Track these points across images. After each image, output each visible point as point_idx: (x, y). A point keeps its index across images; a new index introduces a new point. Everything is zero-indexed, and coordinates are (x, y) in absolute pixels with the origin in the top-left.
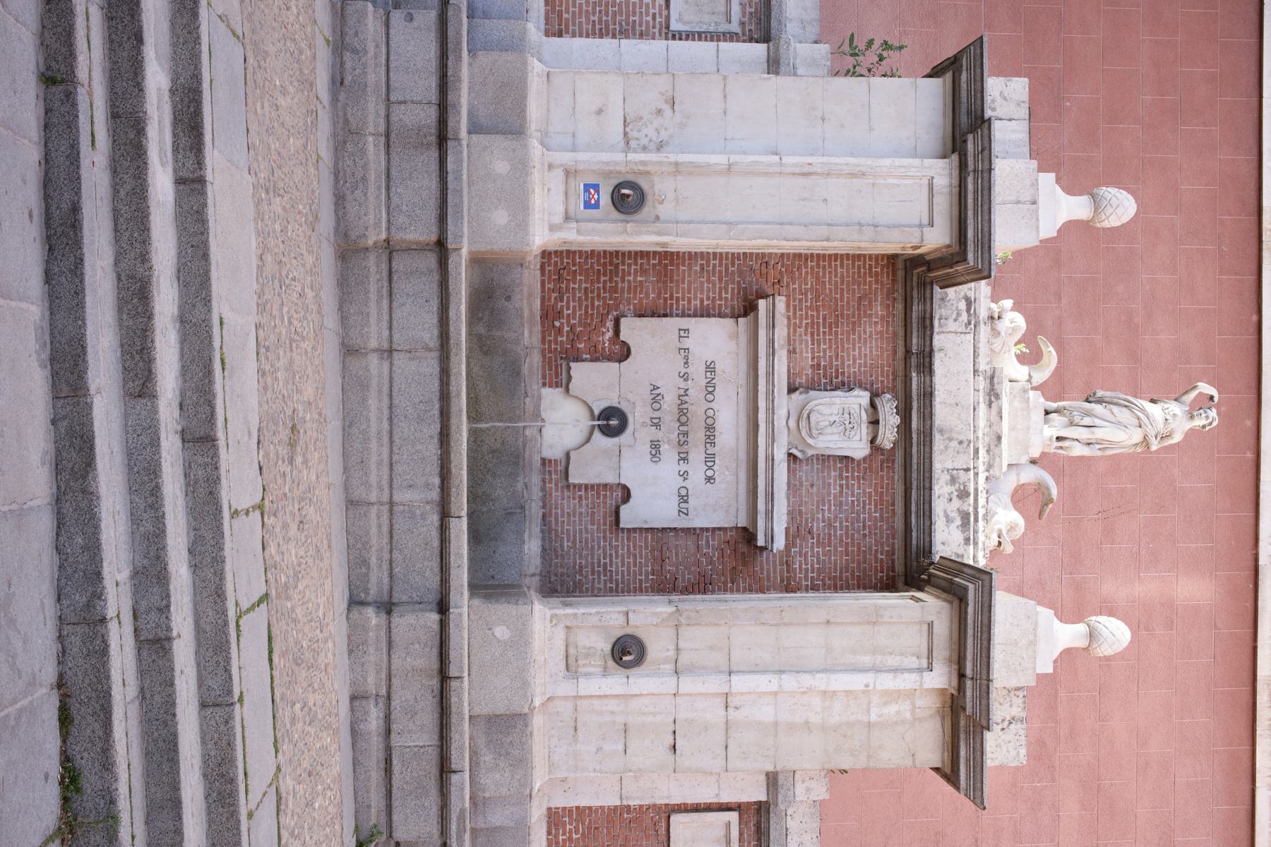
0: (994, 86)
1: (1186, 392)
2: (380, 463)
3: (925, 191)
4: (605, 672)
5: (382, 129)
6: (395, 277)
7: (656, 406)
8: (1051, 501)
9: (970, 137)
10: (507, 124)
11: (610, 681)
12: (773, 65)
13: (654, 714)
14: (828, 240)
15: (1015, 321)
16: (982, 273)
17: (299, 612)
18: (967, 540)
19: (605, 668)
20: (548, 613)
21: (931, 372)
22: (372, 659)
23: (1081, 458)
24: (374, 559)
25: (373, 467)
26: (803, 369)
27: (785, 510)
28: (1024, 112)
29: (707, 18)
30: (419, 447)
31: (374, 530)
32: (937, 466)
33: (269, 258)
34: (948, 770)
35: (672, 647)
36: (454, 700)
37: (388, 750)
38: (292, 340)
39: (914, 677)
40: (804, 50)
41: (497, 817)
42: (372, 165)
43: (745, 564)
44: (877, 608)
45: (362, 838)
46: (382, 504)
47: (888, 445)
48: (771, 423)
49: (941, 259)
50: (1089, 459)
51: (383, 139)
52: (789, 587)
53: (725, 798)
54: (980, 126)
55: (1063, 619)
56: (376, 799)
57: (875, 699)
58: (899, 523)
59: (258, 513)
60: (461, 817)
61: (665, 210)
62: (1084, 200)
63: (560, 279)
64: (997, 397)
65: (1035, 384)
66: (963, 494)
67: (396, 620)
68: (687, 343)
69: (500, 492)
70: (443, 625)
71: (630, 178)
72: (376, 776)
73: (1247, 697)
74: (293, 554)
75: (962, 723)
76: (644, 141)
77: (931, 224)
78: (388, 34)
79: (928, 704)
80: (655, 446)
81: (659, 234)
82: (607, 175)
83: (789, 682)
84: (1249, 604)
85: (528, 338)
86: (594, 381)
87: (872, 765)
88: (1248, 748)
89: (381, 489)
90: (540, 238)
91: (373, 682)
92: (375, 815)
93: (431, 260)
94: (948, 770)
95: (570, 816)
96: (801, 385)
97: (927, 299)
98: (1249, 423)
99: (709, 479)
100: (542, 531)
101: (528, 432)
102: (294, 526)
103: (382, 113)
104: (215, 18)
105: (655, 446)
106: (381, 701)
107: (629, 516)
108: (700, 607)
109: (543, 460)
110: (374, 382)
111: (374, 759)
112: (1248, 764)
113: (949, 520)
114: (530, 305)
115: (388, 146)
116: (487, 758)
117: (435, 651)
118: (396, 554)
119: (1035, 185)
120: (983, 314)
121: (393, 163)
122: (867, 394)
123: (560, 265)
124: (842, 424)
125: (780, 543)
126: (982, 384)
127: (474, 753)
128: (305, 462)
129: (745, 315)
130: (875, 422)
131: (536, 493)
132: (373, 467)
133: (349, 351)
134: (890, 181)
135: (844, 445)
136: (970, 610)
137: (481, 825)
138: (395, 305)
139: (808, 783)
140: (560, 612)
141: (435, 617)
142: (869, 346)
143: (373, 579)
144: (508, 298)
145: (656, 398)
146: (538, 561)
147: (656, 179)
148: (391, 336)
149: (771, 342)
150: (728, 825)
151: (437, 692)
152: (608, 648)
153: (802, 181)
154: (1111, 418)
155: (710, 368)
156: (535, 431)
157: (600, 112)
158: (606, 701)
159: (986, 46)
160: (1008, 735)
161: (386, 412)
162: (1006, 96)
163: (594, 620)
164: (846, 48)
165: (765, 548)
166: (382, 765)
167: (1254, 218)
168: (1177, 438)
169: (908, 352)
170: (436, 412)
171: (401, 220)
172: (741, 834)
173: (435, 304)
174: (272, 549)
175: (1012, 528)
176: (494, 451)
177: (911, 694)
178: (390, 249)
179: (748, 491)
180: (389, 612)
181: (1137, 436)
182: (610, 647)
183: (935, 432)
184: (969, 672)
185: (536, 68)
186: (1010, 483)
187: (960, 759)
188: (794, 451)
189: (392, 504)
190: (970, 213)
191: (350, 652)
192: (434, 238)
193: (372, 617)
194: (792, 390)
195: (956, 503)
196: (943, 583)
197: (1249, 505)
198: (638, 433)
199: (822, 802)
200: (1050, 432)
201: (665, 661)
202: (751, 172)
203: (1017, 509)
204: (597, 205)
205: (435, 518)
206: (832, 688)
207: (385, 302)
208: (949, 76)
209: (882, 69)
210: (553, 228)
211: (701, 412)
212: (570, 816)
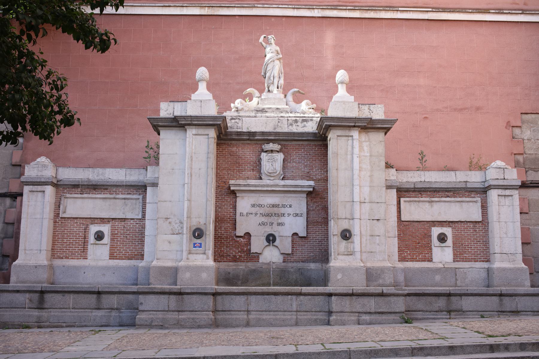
0: (163, 114)
1: (263, 46)
2: (284, 315)
3: (197, 136)
4: (353, 242)
5: (177, 313)
6: (224, 309)
7: (266, 224)
8: (298, 91)
9: (180, 122)
11: (355, 241)
12: (155, 185)
13: (367, 226)
15: (238, 103)
17: (328, 336)
18: (311, 120)
19: (351, 242)
20: (333, 261)
21: (255, 132)
22: (346, 318)
23: (285, 80)
24: (314, 317)
25: (285, 317)
26: (254, 175)
27: (301, 181)
28: (172, 104)
29: (137, 206)
30: (279, 302)
31: (305, 317)
33: (223, 343)
35: (345, 220)
36: (359, 292)
37: (376, 313)
39: (355, 142)
40: (150, 174)
41: (401, 278)
42: (189, 316)
43: (319, 195)
44: (332, 154)
45: (404, 321)
46: (297, 314)
47: (280, 146)
49: (218, 130)
50: (285, 76)
51: (180, 313)
52: (326, 180)
54: (177, 119)
55: (337, 91)
56: (392, 317)
57: (362, 154)
58: (306, 143)
60: (397, 290)
61: (202, 221)
62: (200, 84)
63: (223, 256)
64: (263, 109)
65: (259, 95)
66: (296, 121)
67: (334, 310)
68: (245, 213)
69: (294, 277)
70: (336, 295)
71: (192, 233)
72: (384, 317)
73: (367, 21)
74: (310, 338)
75: (370, 126)
76: (179, 228)
77: (208, 135)
78: (146, 311)
79: (364, 136)
80: (279, 224)
81: (210, 224)
82: (190, 240)
83: (356, 182)
84: (335, 20)
85: (242, 267)
86: (257, 244)
87: (384, 155)
88: (384, 21)
89: (292, 315)
90: (211, 262)
91: (354, 318)
92: (397, 317)
93: (219, 298)
94: (385, 130)
95: (402, 254)
96: (259, 175)
98: (273, 19)
99: (290, 206)
100: (307, 262)
101: (274, 267)
102: (302, 338)
103: (172, 313)
105: (279, 224)
106: (360, 315)
107: (303, 233)
108: (332, 212)
109: (283, 262)
110: (258, 316)
112: (389, 21)
113: (305, 126)
114: (231, 266)
115: (182, 311)
116: (381, 281)
117: (344, 297)
118: (313, 310)
119: (195, 101)
120: (236, 114)
121: (188, 309)
122: (263, 154)
123: (218, 257)
124: (272, 162)
125: (312, 183)
126: (259, 115)
127: (379, 285)
129: (236, 194)
130: (272, 151)
131: (295, 264)
132: (285, 317)
133: (248, 324)
134: (194, 148)
135: (279, 161)
136: (333, 124)
137: (403, 284)
138: (233, 310)
139: (391, 176)
140: (333, 257)
141: (333, 297)
142: (247, 153)
143: (321, 317)
144: (229, 273)
145: (263, 224)
146: (317, 264)
147: (192, 224)
148: (243, 311)
149: (245, 186)
150: (405, 201)
151: (357, 297)
154: (271, 70)
155: (253, 206)
156: (274, 265)
157: (170, 242)
158: (362, 242)
159: (151, 117)
160: (374, 110)
161: (267, 313)
162: (166, 110)
163: (336, 246)
164: (148, 160)
165: (314, 188)
166: (381, 315)
167: (203, 17)
168: (278, 48)
169: (248, 140)
170: (267, 297)
171: (206, 307)
173: (233, 297)
174: (308, 343)
175: (307, 104)
176: (280, 279)
177: (360, 142)
178: (215, 311)
179: (294, 193)
180: (332, 312)
181: (277, 62)
182: (345, 241)
183: (275, 131)
184: (353, 124)
185: (155, 263)
186: (292, 104)
187: (382, 127)
189: (297, 311)
190: (205, 123)
191: (344, 325)
192: (212, 297)
193: (333, 318)
194: (261, 178)
195: (299, 124)
196: (325, 130)
197: (301, 19)
198: (275, 230)
200: (275, 91)
201: (349, 222)
202: (190, 193)
203: (301, 102)
204: (200, 244)
205: (302, 297)
206: (358, 168)
207: (232, 313)
208: (159, 128)
209: (156, 149)
210: (208, 258)
211: (268, 209)
212: (402, 254)
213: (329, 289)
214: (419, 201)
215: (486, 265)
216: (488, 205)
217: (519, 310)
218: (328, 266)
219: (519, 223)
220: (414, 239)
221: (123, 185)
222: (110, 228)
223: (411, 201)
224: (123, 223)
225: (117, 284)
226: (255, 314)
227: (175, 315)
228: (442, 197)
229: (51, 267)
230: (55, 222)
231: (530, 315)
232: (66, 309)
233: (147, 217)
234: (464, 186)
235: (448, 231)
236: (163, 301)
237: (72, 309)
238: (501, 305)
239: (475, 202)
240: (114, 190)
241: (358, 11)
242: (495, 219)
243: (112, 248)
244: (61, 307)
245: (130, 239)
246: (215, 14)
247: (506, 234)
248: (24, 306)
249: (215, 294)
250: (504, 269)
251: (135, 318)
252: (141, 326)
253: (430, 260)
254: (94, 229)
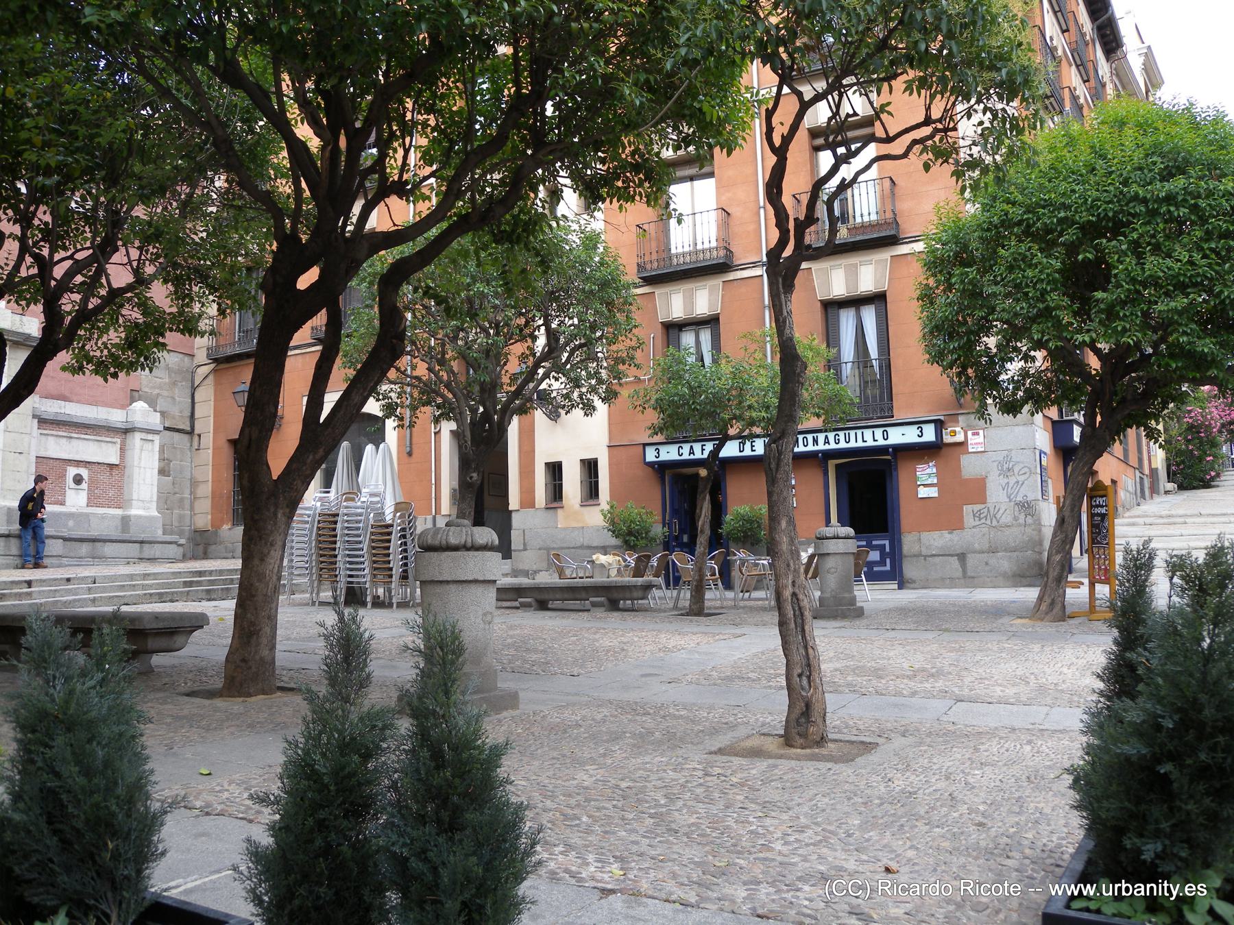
215: (119, 512)
235: (84, 472)
238: (141, 552)
250: (140, 517)
253: (62, 503)
254: (72, 471)
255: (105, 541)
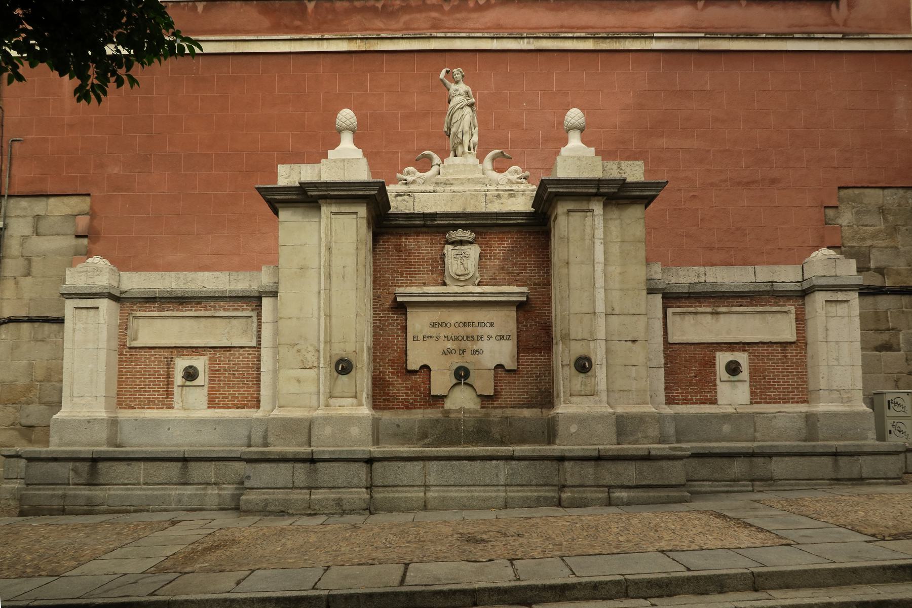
0: (282, 182)
2: (485, 491)
3: (338, 216)
9: (309, 193)
10: (308, 427)
14: (365, 266)
16: (382, 187)
30: (476, 472)
31: (520, 494)
32: (484, 210)
34: (646, 201)
35: (581, 343)
38: (419, 541)
41: (671, 430)
46: (506, 490)
47: (473, 235)
48: (462, 294)
53: (661, 315)
59: (514, 562)
66: (499, 196)
71: (333, 366)
76: (314, 358)
77: (356, 213)
80: (474, 352)
81: (363, 351)
83: (600, 282)
86: (440, 383)
88: (630, 54)
90: (365, 411)
97: (398, 216)
99: (491, 325)
102: (521, 540)
103: (299, 491)
104: (237, 589)
107: (510, 364)
110: (442, 494)
111: (643, 494)
115: (317, 488)
117: (585, 463)
119: (335, 161)
121: (326, 485)
125: (524, 289)
128: (485, 532)
130: (461, 242)
136: (561, 190)
137: (674, 439)
140: (562, 399)
142: (421, 247)
143: (547, 494)
146: (534, 410)
149: (420, 295)
150: (674, 313)
152: (582, 375)
153: (334, 279)
155: (433, 325)
157: (299, 381)
160: (628, 170)
161: (457, 488)
162: (288, 175)
165: (528, 298)
170: (458, 463)
171: (355, 481)
172: (679, 307)
178: (370, 487)
181: (468, 110)
184: (594, 191)
188: (476, 282)
189: (506, 485)
192: (364, 465)
194: (444, 284)
198: (467, 361)
199: (663, 265)
207: (399, 489)
208: (277, 205)
210: (360, 404)
213: (557, 449)
214: (696, 313)
215: (803, 408)
216: (807, 317)
217: (864, 475)
218: (552, 413)
219: (859, 343)
220: (688, 370)
221: (225, 297)
222: (207, 362)
223: (684, 313)
224: (228, 353)
225: (220, 445)
226: (438, 491)
227: (303, 495)
228: (732, 306)
229: (114, 423)
230: (121, 354)
231: (882, 483)
232: (134, 484)
233: (264, 343)
234: (769, 289)
235: (742, 358)
236: (282, 474)
237: (144, 484)
239: (785, 312)
240: (212, 304)
241: (591, 40)
242: (821, 337)
243: (211, 392)
244: (126, 482)
245: (237, 376)
246: (372, 49)
247: (837, 360)
248: (66, 482)
249: (370, 461)
250: (835, 415)
251: (239, 499)
252: (248, 512)
253: (714, 402)
254: (181, 364)
255: (770, 456)
